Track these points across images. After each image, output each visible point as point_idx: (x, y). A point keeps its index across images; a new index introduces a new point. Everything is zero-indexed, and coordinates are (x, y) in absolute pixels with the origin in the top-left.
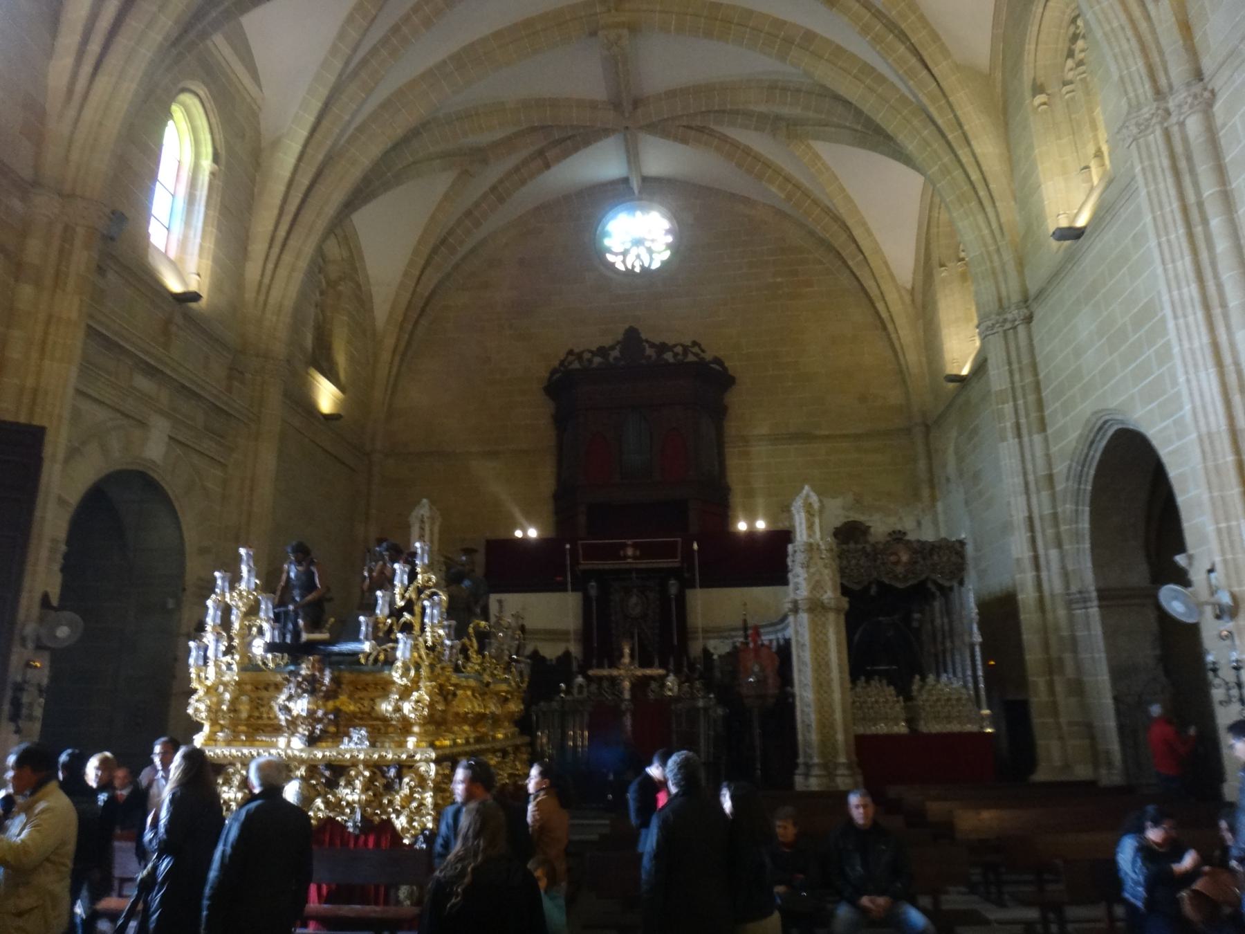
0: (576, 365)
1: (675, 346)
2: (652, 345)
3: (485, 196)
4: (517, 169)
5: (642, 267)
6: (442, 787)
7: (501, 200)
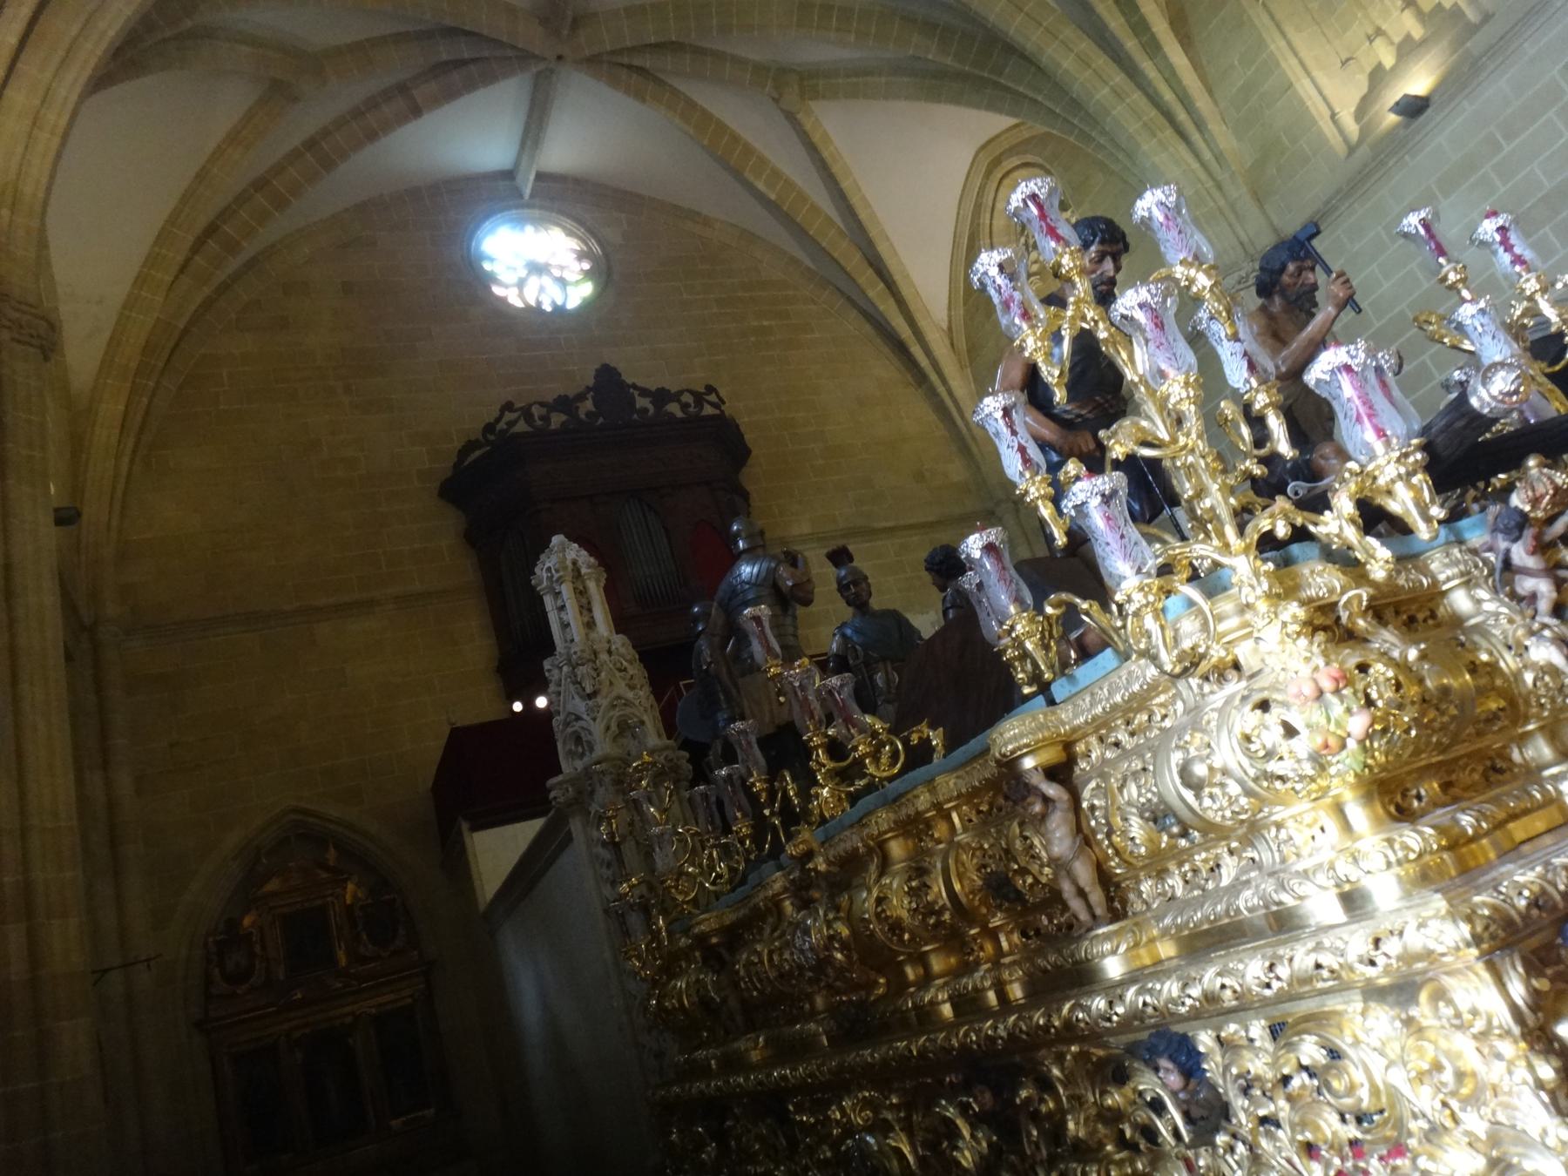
0: (521, 427)
1: (681, 392)
2: (644, 392)
3: (295, 156)
4: (357, 113)
5: (554, 303)
6: (1407, 731)
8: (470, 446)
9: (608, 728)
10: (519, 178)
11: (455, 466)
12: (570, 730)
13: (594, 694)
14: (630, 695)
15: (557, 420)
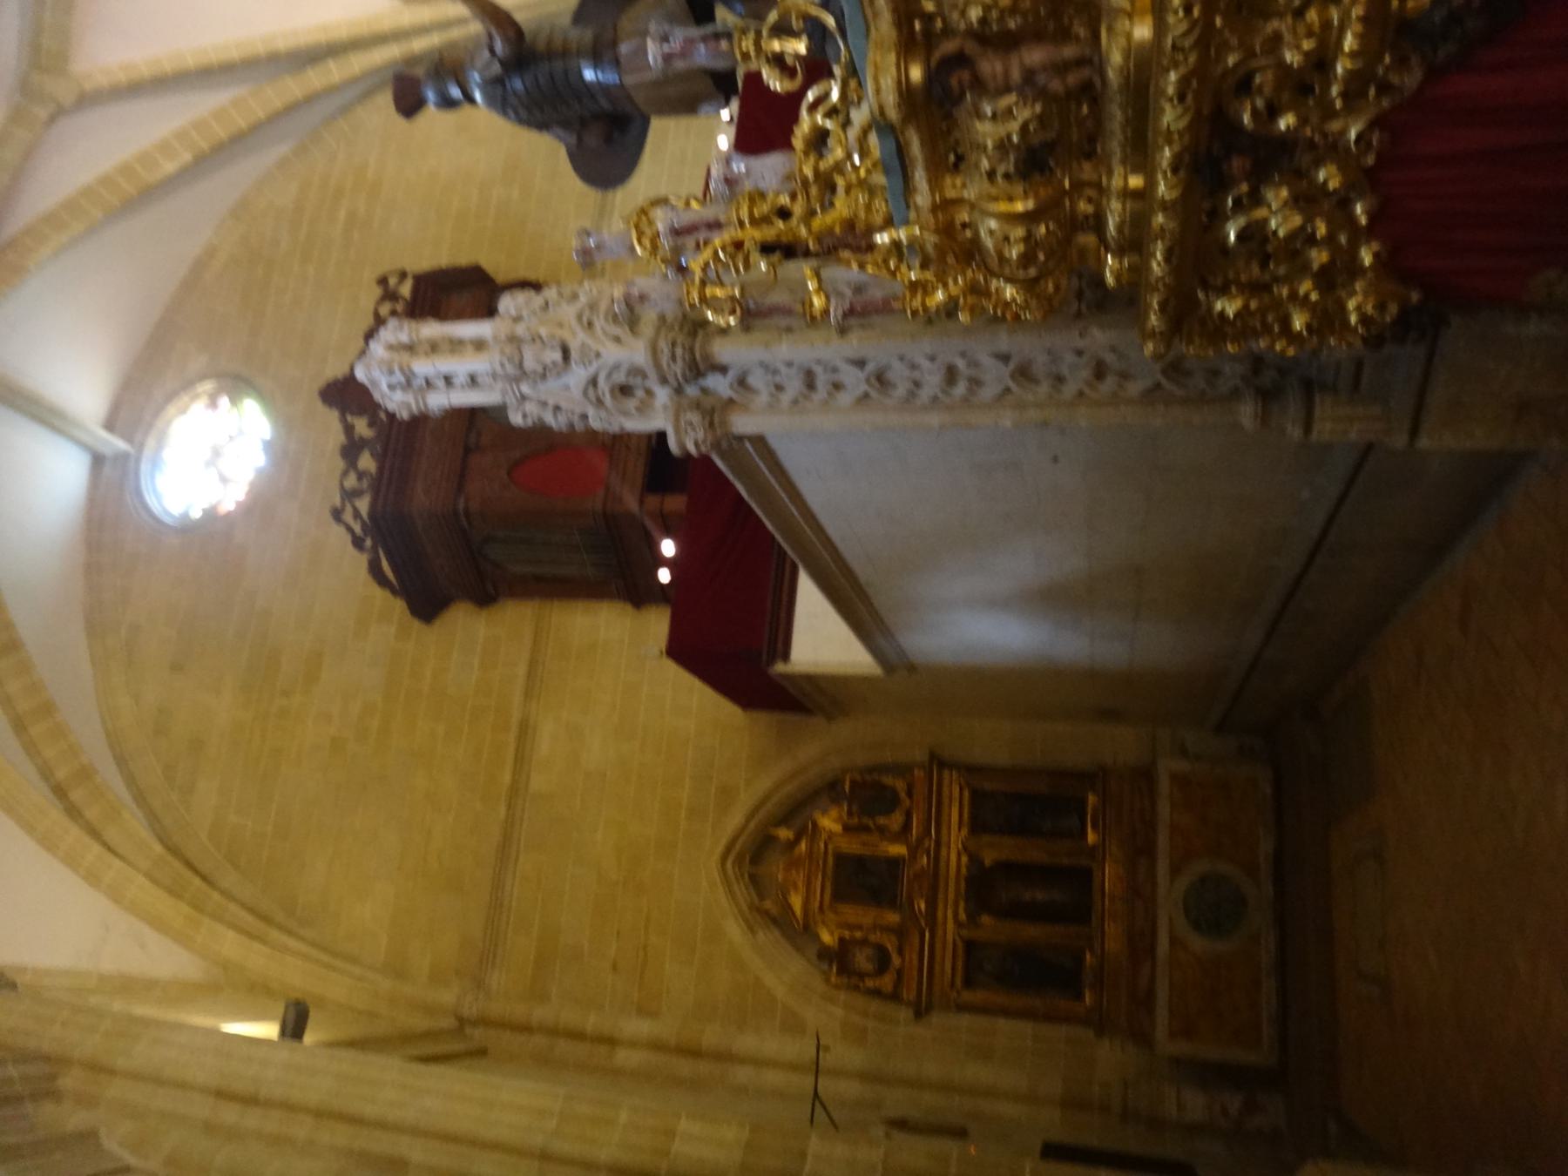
0: (363, 505)
7: (47, 709)
8: (375, 570)
9: (617, 340)
10: (106, 451)
11: (394, 592)
12: (608, 400)
13: (566, 352)
14: (583, 299)
15: (367, 462)
